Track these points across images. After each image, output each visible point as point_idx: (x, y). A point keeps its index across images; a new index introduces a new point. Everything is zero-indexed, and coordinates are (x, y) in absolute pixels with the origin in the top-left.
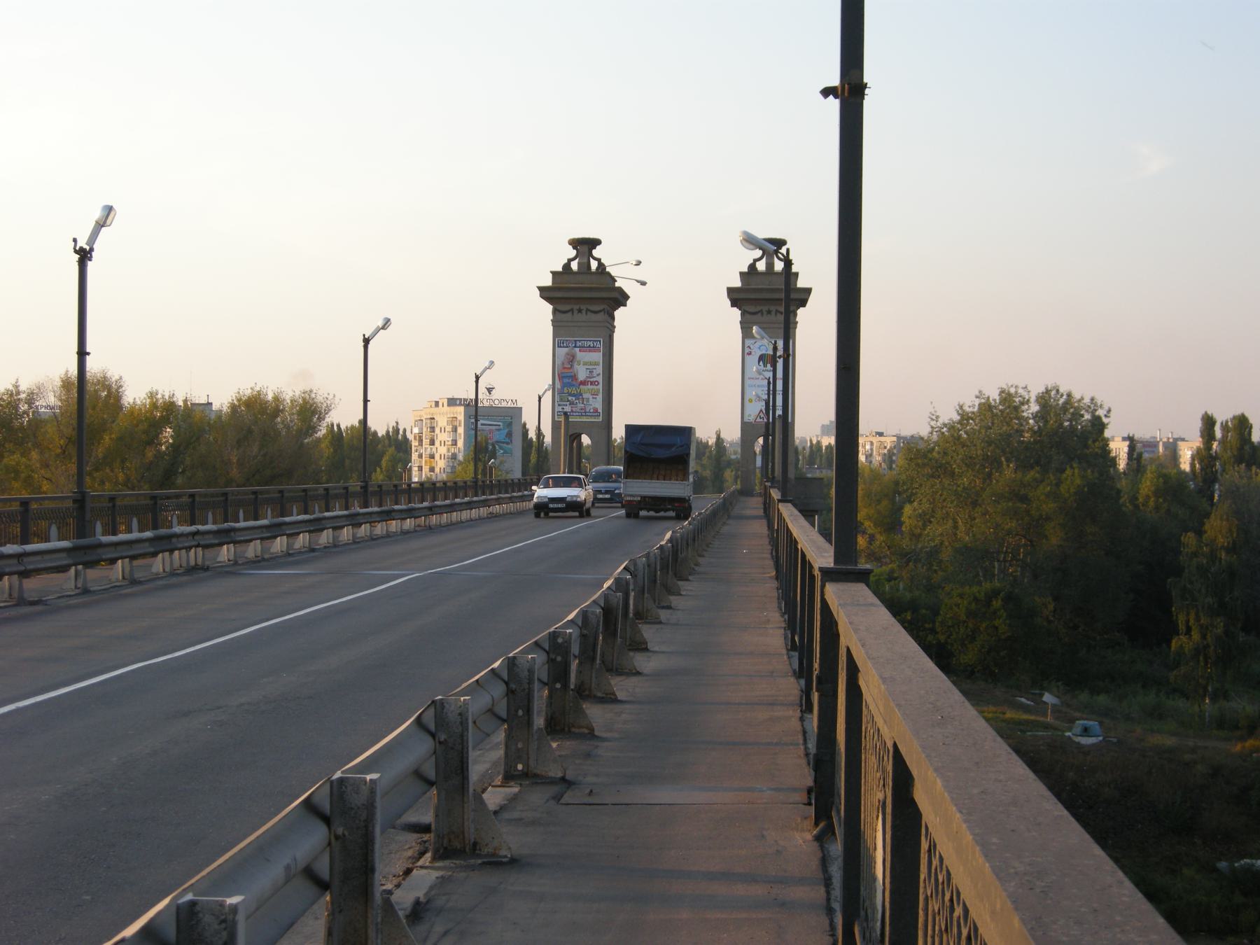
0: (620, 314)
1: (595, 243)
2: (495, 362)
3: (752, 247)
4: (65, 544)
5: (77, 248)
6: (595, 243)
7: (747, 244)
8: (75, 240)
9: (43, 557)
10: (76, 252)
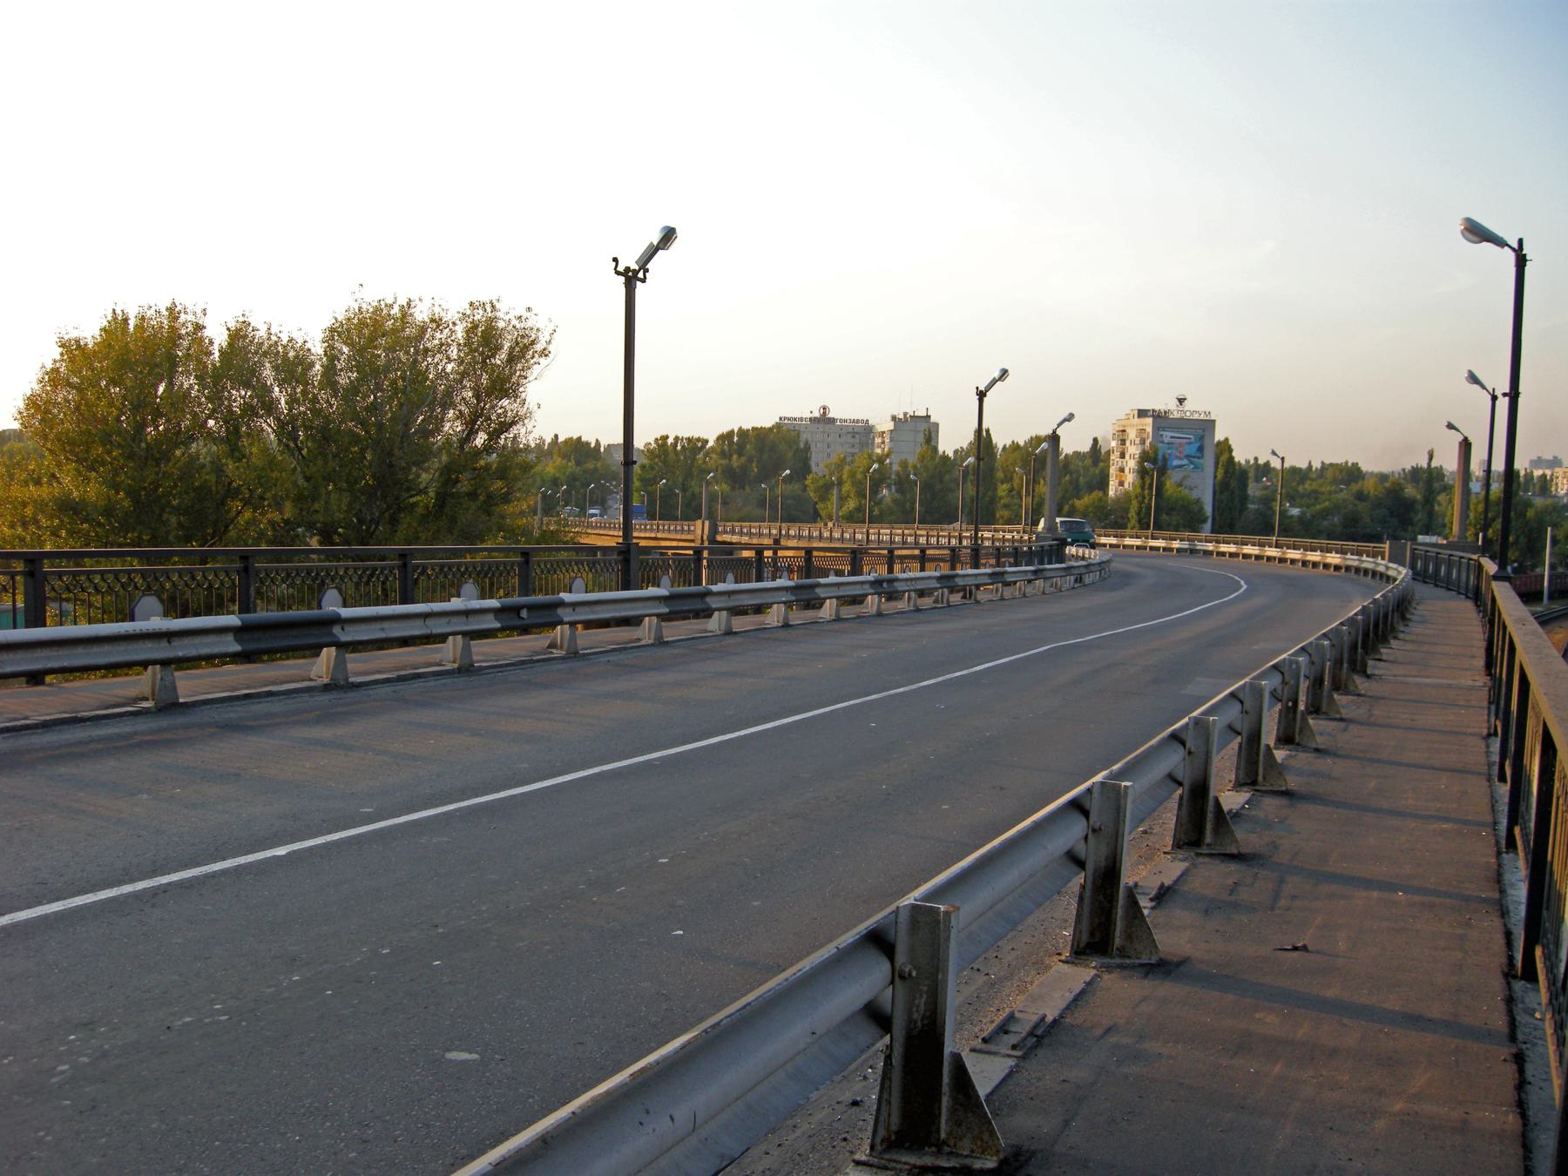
2: (1010, 372)
3: (1475, 239)
7: (1467, 234)
8: (615, 260)
9: (574, 610)
10: (618, 273)
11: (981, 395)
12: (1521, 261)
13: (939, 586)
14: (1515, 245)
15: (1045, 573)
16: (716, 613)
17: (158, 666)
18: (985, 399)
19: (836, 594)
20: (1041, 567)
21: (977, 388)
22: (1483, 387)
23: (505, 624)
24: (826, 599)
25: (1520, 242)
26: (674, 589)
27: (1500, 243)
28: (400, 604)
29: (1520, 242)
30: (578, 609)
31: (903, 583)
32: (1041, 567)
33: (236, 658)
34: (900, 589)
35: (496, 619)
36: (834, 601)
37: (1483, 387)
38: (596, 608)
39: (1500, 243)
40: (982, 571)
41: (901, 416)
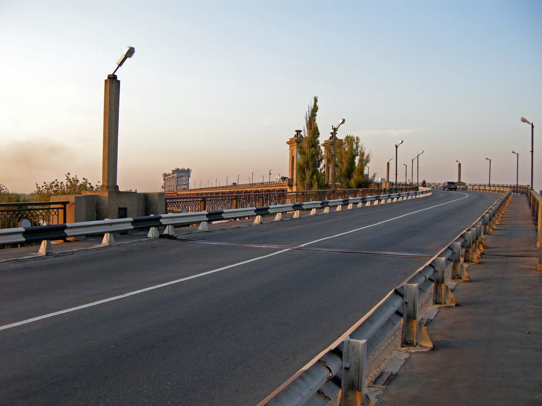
2: (345, 120)
4: (361, 198)
5: (333, 128)
8: (332, 126)
10: (333, 129)
11: (413, 160)
12: (533, 127)
13: (256, 214)
14: (531, 124)
15: (391, 196)
16: (313, 209)
17: (260, 216)
18: (398, 148)
19: (171, 223)
20: (390, 194)
21: (332, 126)
22: (516, 153)
23: (136, 227)
24: (166, 225)
25: (532, 123)
26: (32, 227)
27: (489, 159)
28: (13, 228)
29: (532, 123)
30: (317, 205)
31: (351, 201)
32: (390, 194)
33: (22, 244)
34: (163, 223)
35: (24, 237)
36: (352, 204)
37: (516, 153)
38: (175, 219)
39: (489, 159)
40: (357, 198)
41: (331, 135)
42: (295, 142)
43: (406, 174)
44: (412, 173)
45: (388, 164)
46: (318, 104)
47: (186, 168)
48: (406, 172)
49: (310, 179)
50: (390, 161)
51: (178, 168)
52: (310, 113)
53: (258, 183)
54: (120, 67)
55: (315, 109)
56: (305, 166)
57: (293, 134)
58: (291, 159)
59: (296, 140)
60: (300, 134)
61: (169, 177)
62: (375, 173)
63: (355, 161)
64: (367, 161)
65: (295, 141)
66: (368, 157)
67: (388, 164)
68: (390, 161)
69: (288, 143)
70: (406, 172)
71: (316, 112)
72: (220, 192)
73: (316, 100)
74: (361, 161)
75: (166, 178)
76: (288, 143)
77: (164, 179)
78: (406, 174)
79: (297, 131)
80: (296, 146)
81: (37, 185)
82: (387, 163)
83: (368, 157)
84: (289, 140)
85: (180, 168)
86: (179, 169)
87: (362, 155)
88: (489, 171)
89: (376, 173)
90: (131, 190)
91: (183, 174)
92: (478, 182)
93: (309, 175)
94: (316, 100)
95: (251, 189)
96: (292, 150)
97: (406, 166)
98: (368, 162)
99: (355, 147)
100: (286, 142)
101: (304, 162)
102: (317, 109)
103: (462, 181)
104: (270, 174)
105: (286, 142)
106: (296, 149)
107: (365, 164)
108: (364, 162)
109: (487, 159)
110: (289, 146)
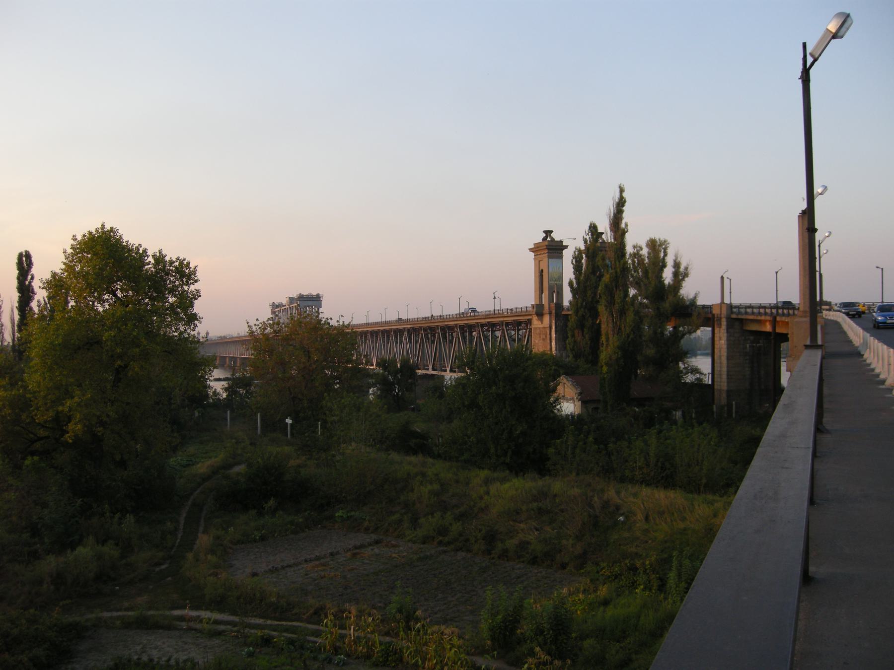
0: (564, 251)
1: (552, 232)
6: (552, 232)
11: (777, 273)
27: (880, 268)
39: (880, 268)
41: (544, 235)
42: (546, 248)
43: (730, 292)
44: (777, 291)
45: (722, 278)
46: (624, 195)
47: (314, 293)
48: (730, 289)
49: (622, 303)
50: (724, 273)
51: (301, 294)
52: (615, 209)
53: (450, 315)
54: (804, 206)
55: (621, 203)
56: (614, 284)
57: (539, 237)
58: (538, 274)
59: (546, 246)
60: (550, 236)
61: (283, 308)
62: (697, 292)
63: (18, 272)
64: (686, 275)
65: (545, 247)
66: (686, 268)
67: (722, 278)
68: (724, 273)
69: (531, 250)
70: (730, 289)
71: (623, 206)
72: (391, 329)
73: (622, 191)
74: (676, 274)
75: (277, 310)
76: (531, 250)
77: (272, 311)
78: (730, 292)
79: (546, 232)
80: (547, 254)
81: (248, 323)
82: (721, 276)
83: (686, 268)
84: (533, 246)
85: (305, 293)
86: (303, 295)
87: (677, 265)
88: (881, 284)
89: (699, 292)
90: (239, 334)
91: (310, 303)
92: (360, 323)
93: (620, 298)
94: (622, 191)
95: (367, 329)
96: (539, 261)
97: (730, 280)
98: (687, 277)
99: (662, 255)
100: (529, 249)
101: (612, 279)
102: (625, 202)
103: (825, 299)
104: (494, 298)
105: (529, 249)
106: (547, 259)
107: (683, 279)
108: (680, 275)
109: (877, 267)
110: (533, 254)
